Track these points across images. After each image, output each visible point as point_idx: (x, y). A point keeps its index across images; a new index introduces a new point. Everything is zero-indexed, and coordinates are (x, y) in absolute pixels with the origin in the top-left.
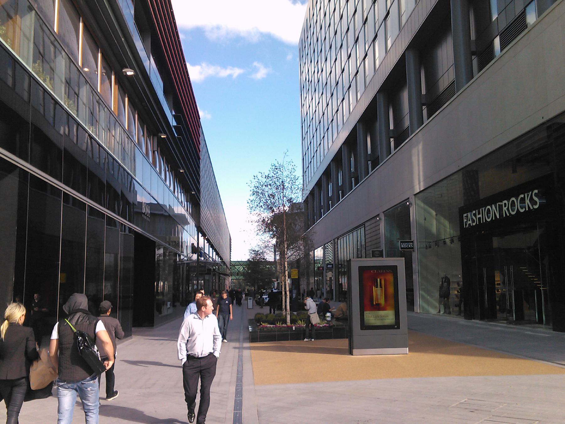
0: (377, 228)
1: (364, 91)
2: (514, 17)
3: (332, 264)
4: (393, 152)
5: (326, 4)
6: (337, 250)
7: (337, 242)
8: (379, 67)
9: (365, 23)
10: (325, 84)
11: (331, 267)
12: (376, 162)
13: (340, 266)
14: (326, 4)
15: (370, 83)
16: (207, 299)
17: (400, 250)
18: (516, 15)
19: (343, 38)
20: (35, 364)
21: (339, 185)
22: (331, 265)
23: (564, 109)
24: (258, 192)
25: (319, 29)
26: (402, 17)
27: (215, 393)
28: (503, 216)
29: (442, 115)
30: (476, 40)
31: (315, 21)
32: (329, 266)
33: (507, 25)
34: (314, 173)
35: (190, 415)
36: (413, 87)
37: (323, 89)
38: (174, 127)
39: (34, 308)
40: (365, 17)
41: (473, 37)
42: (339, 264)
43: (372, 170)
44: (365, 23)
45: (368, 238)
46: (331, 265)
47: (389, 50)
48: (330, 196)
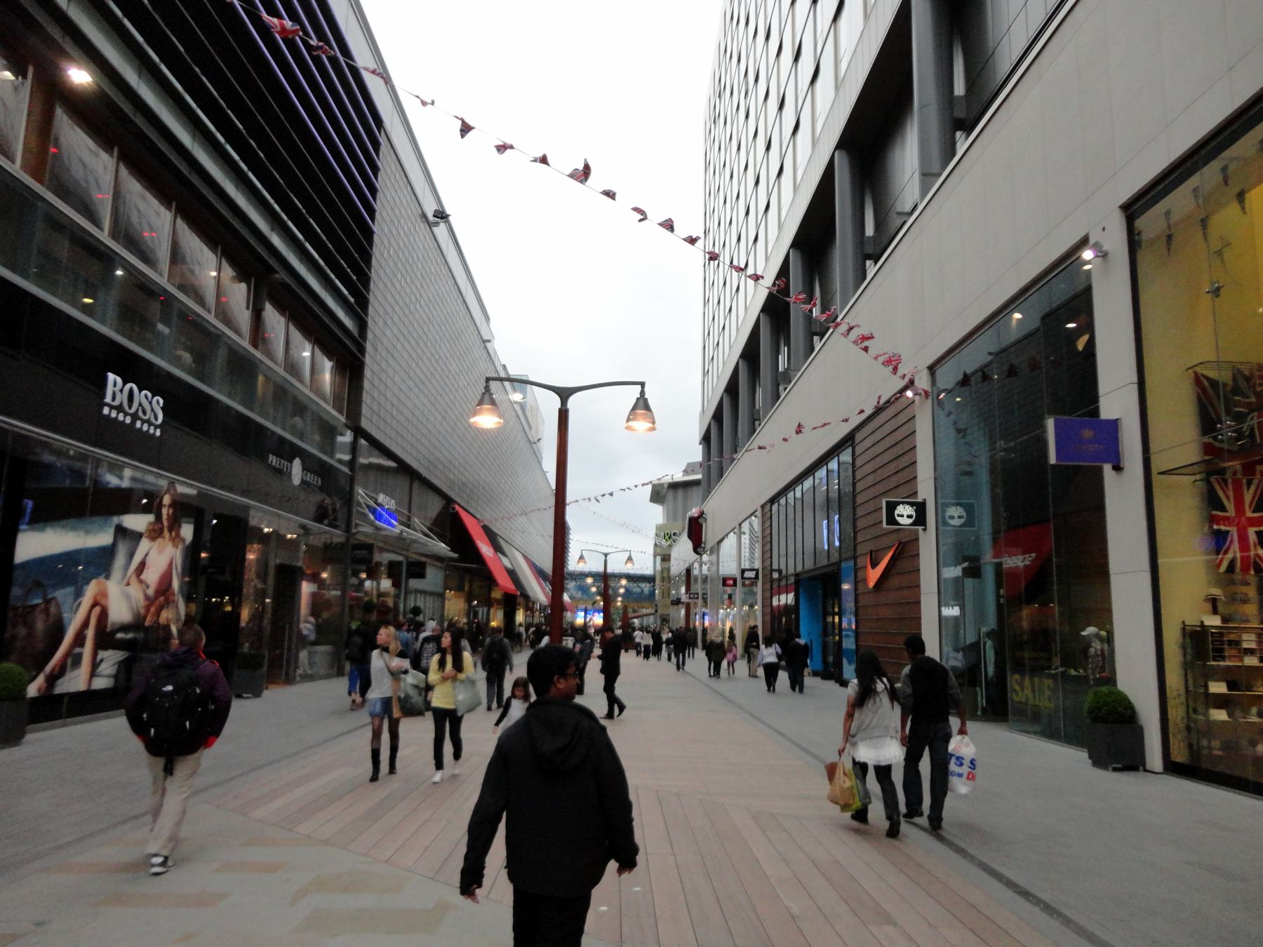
0: (905, 461)
3: (757, 571)
5: (727, 184)
6: (769, 532)
7: (771, 510)
11: (754, 576)
13: (776, 575)
14: (727, 184)
16: (81, 182)
19: (759, 222)
22: (754, 573)
24: (387, 703)
25: (729, 177)
27: (717, 897)
28: (1236, 407)
30: (966, 95)
32: (747, 574)
35: (1237, 404)
37: (714, 275)
38: (276, 272)
46: (754, 573)
48: (780, 369)
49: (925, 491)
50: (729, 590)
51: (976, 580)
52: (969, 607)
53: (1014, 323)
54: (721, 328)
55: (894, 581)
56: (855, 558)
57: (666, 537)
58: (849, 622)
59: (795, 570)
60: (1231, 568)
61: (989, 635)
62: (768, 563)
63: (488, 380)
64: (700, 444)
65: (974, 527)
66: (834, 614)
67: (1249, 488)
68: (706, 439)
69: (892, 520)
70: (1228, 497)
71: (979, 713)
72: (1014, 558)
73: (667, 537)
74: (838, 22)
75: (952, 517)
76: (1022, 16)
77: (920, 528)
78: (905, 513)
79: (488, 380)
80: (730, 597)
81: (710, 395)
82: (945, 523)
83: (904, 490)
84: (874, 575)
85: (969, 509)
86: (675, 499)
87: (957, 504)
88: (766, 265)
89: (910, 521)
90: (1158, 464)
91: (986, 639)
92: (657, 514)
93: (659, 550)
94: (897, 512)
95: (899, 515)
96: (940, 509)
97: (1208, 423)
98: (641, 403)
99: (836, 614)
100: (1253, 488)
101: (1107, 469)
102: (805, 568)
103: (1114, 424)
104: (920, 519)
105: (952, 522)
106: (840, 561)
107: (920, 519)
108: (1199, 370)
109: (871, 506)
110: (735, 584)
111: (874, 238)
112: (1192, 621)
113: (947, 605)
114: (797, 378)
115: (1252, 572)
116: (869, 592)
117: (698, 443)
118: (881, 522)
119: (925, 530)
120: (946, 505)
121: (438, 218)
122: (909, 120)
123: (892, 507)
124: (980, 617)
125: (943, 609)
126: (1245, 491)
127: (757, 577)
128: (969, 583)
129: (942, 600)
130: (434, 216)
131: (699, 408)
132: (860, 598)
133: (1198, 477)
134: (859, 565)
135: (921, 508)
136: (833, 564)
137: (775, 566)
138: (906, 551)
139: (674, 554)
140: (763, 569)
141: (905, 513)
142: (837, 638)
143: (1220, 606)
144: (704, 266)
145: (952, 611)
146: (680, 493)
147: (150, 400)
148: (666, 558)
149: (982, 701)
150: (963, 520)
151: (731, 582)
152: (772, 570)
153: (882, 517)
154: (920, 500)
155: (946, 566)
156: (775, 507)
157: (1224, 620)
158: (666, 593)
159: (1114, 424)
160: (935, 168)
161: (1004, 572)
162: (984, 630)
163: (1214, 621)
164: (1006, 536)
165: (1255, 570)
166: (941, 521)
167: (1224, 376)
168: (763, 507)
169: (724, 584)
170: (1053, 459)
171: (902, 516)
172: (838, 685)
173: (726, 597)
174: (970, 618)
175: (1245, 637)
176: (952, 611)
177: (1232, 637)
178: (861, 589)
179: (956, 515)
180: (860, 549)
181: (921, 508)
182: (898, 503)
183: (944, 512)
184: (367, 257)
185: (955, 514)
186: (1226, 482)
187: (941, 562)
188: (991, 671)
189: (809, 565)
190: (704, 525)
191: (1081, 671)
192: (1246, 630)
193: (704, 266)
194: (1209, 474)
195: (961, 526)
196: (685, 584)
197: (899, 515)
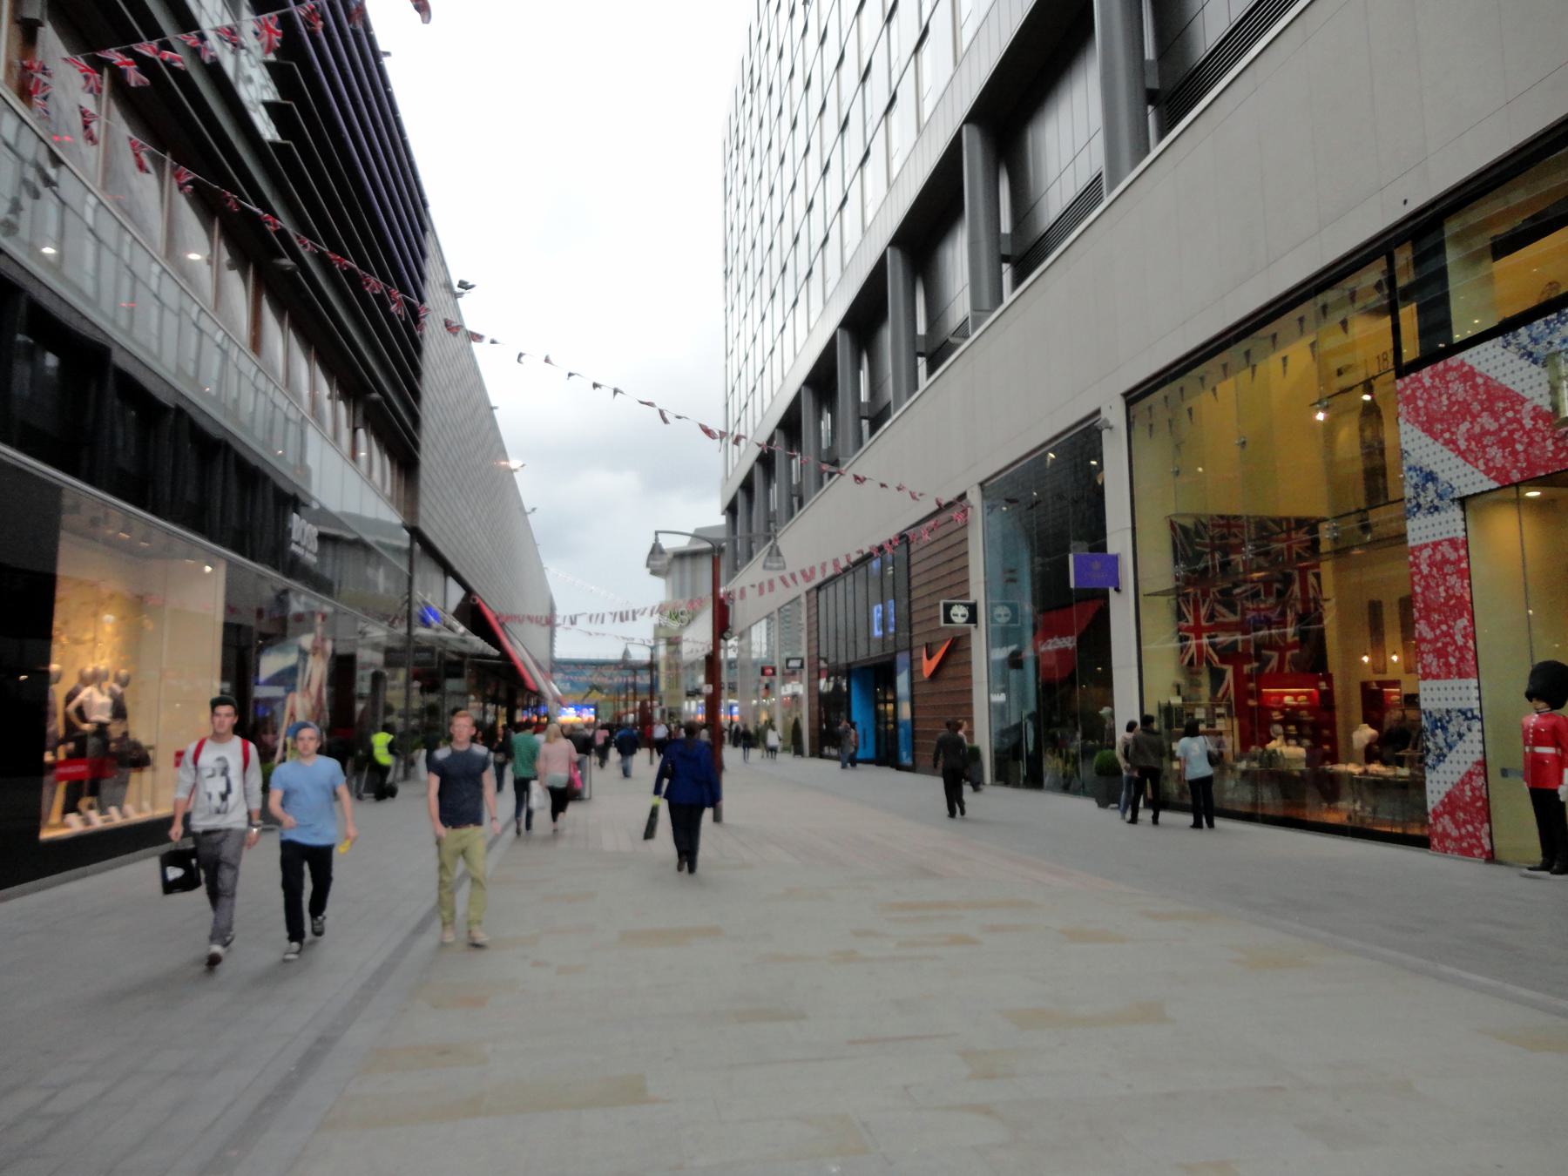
0: (956, 565)
1: (887, 196)
2: (1228, 24)
4: (1008, 298)
7: (817, 597)
8: (873, 221)
9: (864, 79)
10: (768, 246)
12: (878, 418)
15: (983, 33)
17: (942, 624)
18: (1078, 190)
19: (797, 168)
20: (1549, 389)
21: (999, 228)
22: (799, 661)
23: (1565, 113)
26: (963, 30)
29: (1052, 275)
30: (1011, 234)
31: (734, 167)
33: (1231, 24)
34: (809, 331)
36: (784, 480)
39: (651, 732)
40: (809, 200)
41: (1149, 53)
42: (819, 658)
43: (1161, 137)
44: (864, 79)
45: (919, 575)
47: (968, 49)
49: (977, 593)
50: (766, 680)
51: (1019, 671)
52: (1013, 696)
53: (1049, 460)
54: (750, 390)
55: (949, 672)
56: (911, 649)
57: (675, 614)
58: (905, 711)
59: (847, 659)
60: (1191, 663)
61: (1030, 716)
62: (814, 652)
63: (657, 533)
64: (723, 514)
65: (1017, 622)
66: (886, 702)
67: (1203, 604)
68: (731, 509)
69: (948, 619)
70: (1189, 611)
71: (1021, 782)
72: (1064, 639)
73: (673, 616)
74: (889, 117)
75: (1000, 616)
76: (1057, 183)
77: (972, 625)
78: (959, 613)
79: (657, 533)
80: (767, 687)
81: (736, 461)
82: (993, 620)
83: (955, 591)
84: (928, 667)
85: (1014, 609)
86: (682, 572)
87: (1003, 604)
88: (808, 339)
89: (964, 619)
90: (1144, 589)
91: (1027, 720)
92: (657, 591)
93: (662, 632)
94: (952, 612)
95: (954, 615)
96: (990, 609)
97: (1178, 555)
98: (774, 551)
99: (890, 702)
100: (1206, 605)
101: (1112, 590)
102: (859, 655)
103: (1115, 558)
104: (973, 617)
105: (999, 620)
106: (896, 653)
107: (973, 617)
108: (1174, 519)
109: (926, 602)
110: (774, 673)
111: (926, 337)
112: (1164, 702)
113: (995, 693)
114: (848, 465)
115: (1204, 665)
116: (923, 682)
117: (720, 513)
118: (938, 617)
119: (976, 627)
120: (994, 606)
121: (463, 288)
122: (960, 229)
123: (948, 608)
124: (1023, 700)
125: (991, 695)
126: (1201, 606)
127: (802, 666)
128: (1013, 674)
129: (991, 689)
130: (459, 286)
131: (720, 473)
132: (916, 688)
133: (1171, 597)
134: (915, 656)
135: (973, 609)
136: (888, 655)
137: (823, 654)
138: (958, 646)
139: (687, 634)
140: (809, 658)
141: (959, 613)
142: (891, 726)
143: (1182, 690)
144: (726, 311)
145: (1000, 698)
146: (688, 563)
147: (1478, 845)
148: (674, 643)
149: (1023, 772)
150: (1008, 619)
151: (770, 671)
152: (819, 658)
153: (938, 611)
154: (971, 601)
155: (993, 647)
156: (822, 594)
157: (1184, 700)
158: (674, 681)
159: (1115, 558)
160: (986, 304)
161: (1468, 253)
162: (1025, 713)
163: (1176, 701)
164: (1044, 630)
165: (1206, 663)
166: (991, 618)
167: (1189, 523)
168: (808, 593)
169: (763, 673)
170: (1072, 585)
171: (956, 615)
172: (894, 770)
173: (762, 687)
174: (1014, 703)
175: (1197, 710)
176: (1000, 698)
177: (1189, 711)
178: (916, 680)
179: (1002, 613)
180: (916, 642)
181: (973, 609)
182: (953, 605)
183: (992, 612)
184: (419, 349)
185: (1002, 612)
186: (1188, 601)
187: (990, 643)
188: (1031, 748)
189: (862, 653)
190: (731, 607)
191: (1097, 742)
192: (1199, 706)
193: (726, 311)
194: (1178, 596)
195: (1008, 623)
196: (704, 671)
197: (954, 615)
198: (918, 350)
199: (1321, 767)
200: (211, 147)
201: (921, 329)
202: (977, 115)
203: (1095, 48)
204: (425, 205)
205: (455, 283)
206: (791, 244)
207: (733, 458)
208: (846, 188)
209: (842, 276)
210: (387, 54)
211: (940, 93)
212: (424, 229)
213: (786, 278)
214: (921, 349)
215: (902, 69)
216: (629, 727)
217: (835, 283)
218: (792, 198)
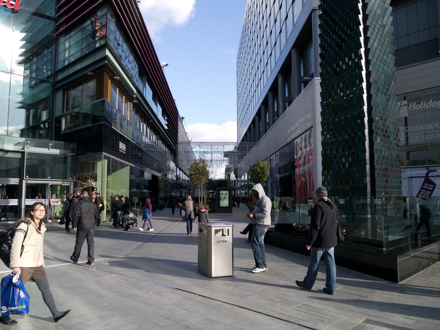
21: (275, 110)
43: (304, 88)
81: (252, 110)
198: (301, 81)
199: (190, 197)
200: (84, 12)
201: (287, 95)
202: (295, 46)
203: (312, 44)
204: (178, 112)
205: (181, 118)
206: (273, 23)
207: (258, 95)
208: (276, 38)
209: (293, 28)
210: (175, 100)
211: (298, 16)
212: (178, 116)
213: (276, 24)
214: (286, 100)
215: (289, 7)
216: (265, 184)
217: (278, 57)
218: (260, 49)
